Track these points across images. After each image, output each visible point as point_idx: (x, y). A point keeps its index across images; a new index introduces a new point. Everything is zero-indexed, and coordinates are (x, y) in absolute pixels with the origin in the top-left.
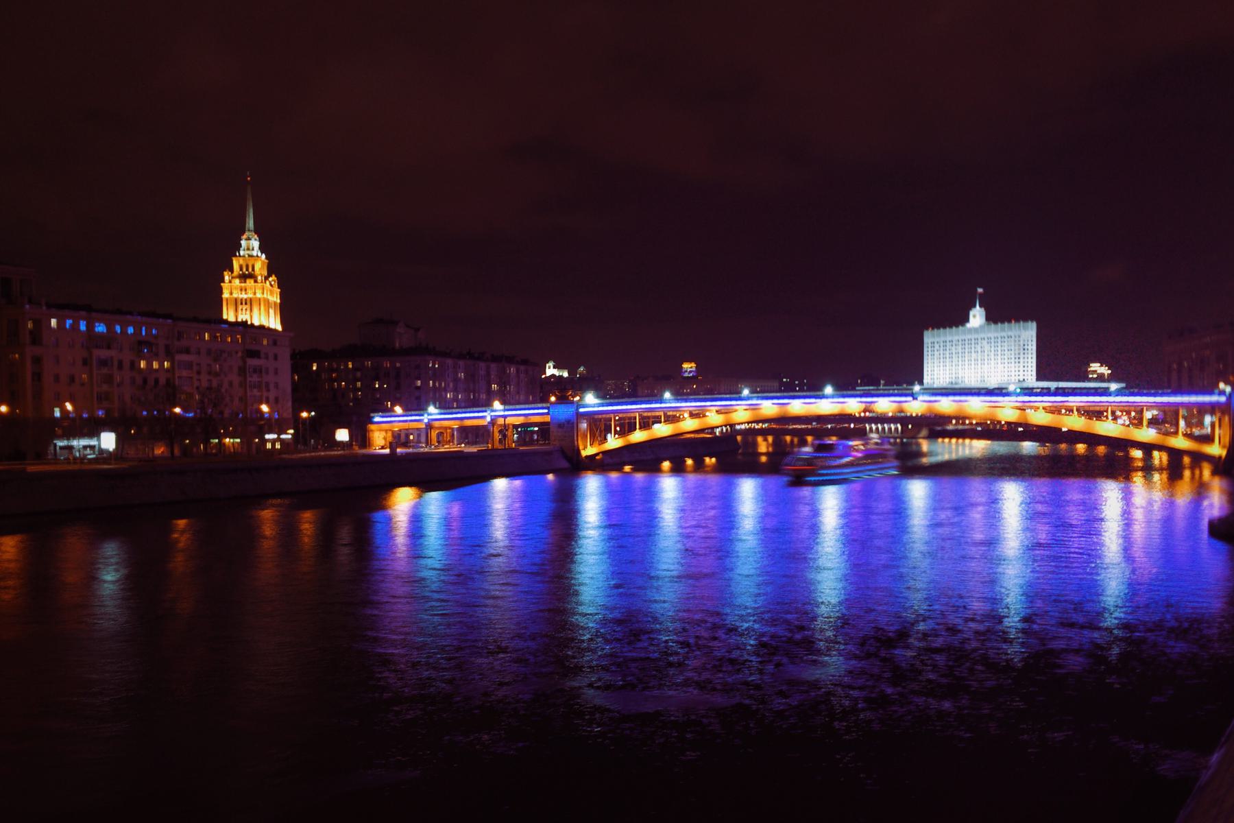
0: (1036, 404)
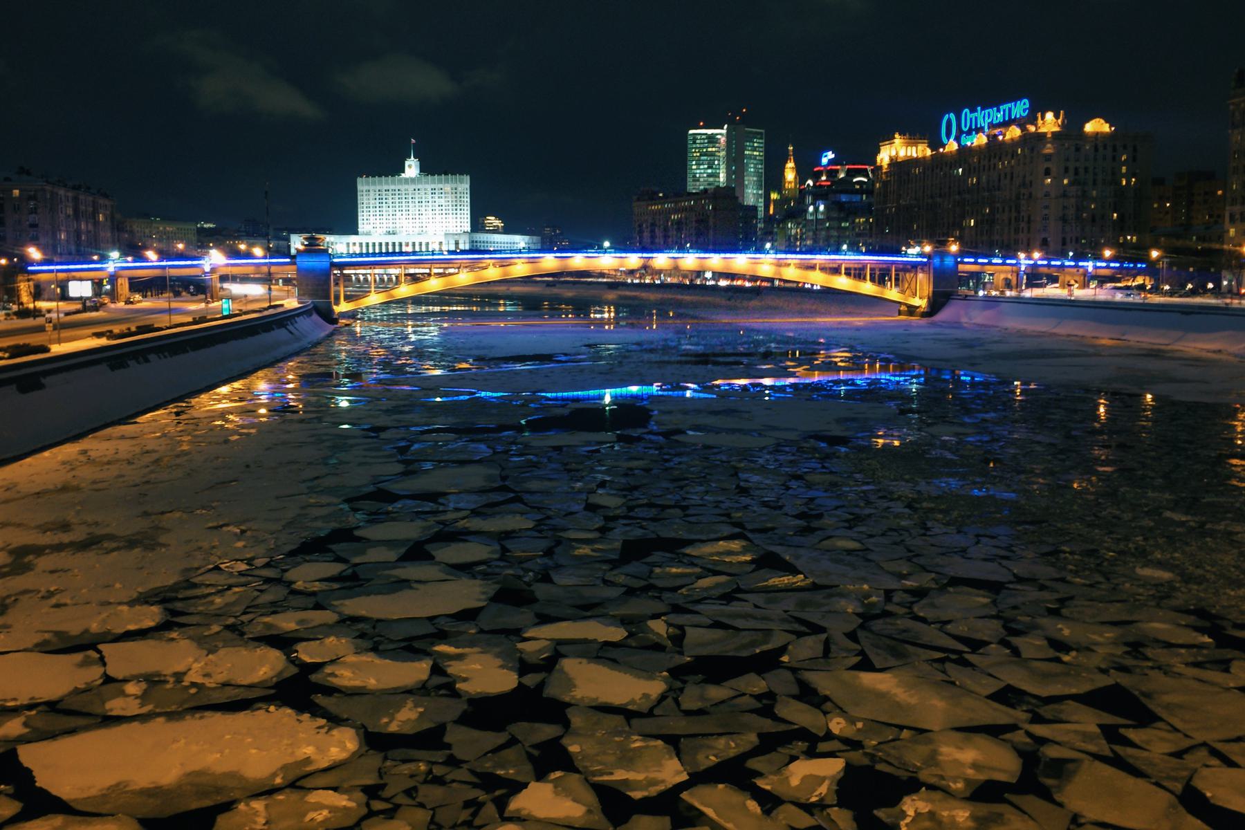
0: (789, 261)
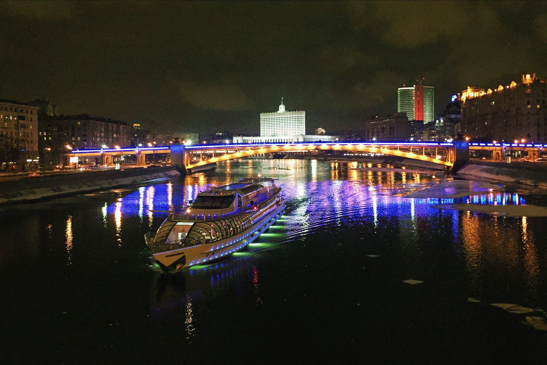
0: (384, 146)
